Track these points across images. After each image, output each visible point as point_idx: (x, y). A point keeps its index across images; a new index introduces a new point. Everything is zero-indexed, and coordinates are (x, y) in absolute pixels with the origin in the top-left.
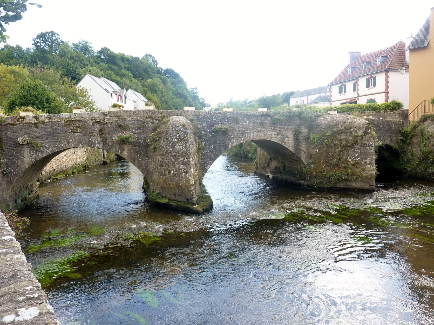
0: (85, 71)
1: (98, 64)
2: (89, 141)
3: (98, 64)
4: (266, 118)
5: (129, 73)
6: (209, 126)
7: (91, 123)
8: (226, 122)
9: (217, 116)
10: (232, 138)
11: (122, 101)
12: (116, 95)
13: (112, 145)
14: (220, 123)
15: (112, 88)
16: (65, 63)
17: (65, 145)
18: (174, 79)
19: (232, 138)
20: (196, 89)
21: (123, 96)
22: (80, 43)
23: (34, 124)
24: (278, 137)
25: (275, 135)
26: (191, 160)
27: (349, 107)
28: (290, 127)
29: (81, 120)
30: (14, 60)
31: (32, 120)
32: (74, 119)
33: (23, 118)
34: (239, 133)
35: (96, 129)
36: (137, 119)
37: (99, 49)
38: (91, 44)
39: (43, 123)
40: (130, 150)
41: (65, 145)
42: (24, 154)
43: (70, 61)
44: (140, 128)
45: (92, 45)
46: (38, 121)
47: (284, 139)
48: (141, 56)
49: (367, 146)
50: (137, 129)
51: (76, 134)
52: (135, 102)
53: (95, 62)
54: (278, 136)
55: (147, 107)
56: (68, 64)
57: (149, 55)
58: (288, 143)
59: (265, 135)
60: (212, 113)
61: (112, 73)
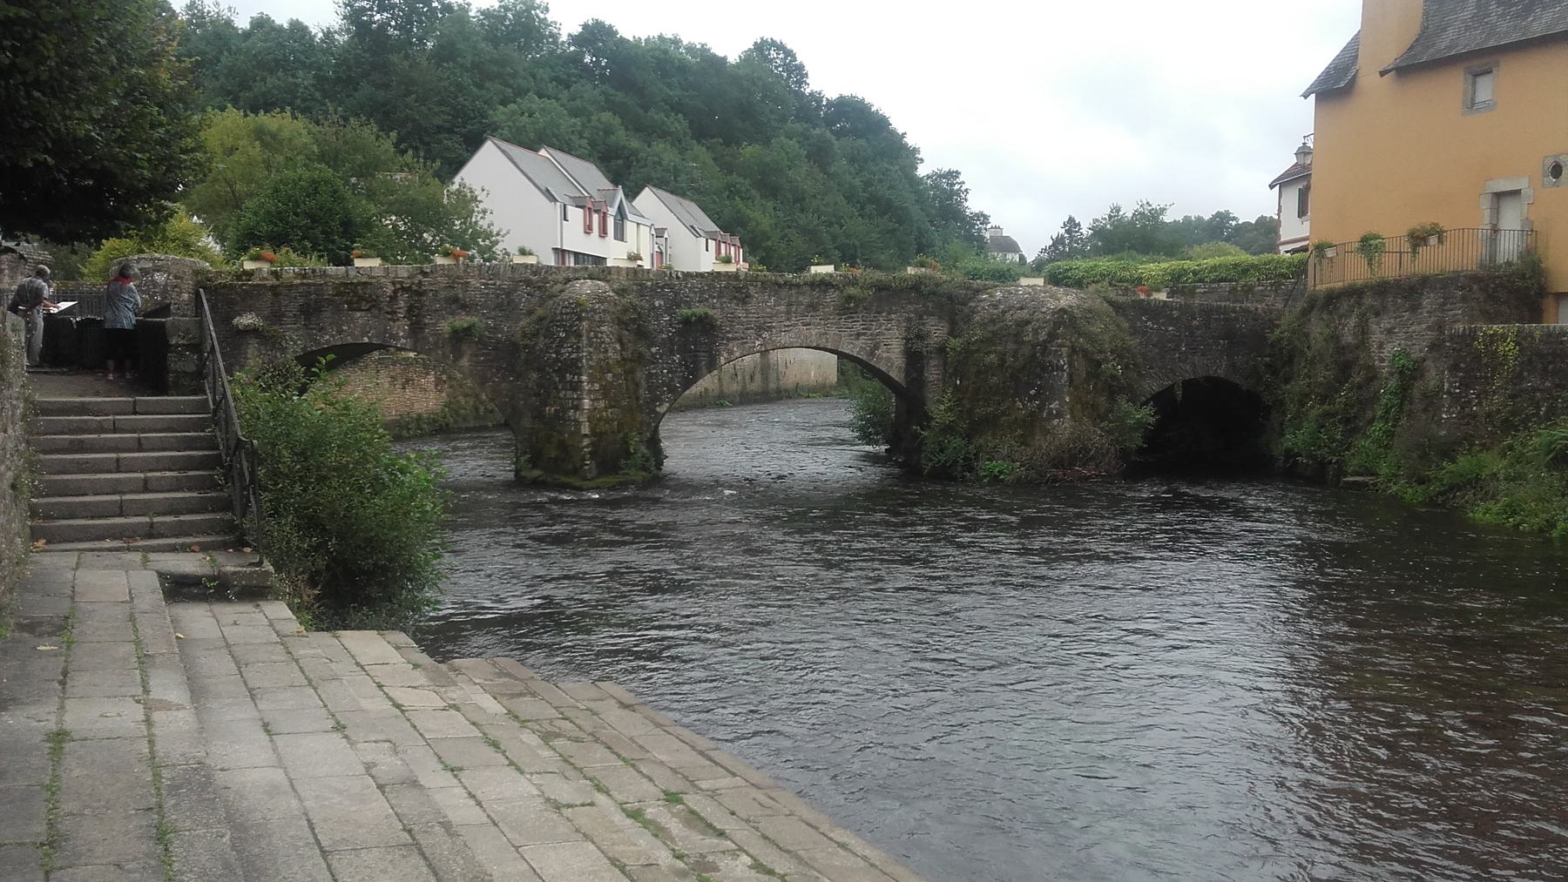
0: (513, 113)
1: (568, 87)
2: (386, 331)
3: (568, 87)
4: (825, 292)
5: (678, 124)
6: (671, 308)
7: (389, 290)
8: (714, 298)
9: (692, 284)
10: (729, 339)
11: (603, 233)
12: (581, 210)
13: (436, 343)
14: (699, 302)
15: (573, 181)
16: (446, 83)
17: (333, 336)
18: (861, 142)
19: (729, 339)
20: (952, 175)
21: (612, 211)
22: (507, 9)
23: (273, 288)
24: (860, 343)
25: (851, 335)
26: (584, 378)
27: (1236, 266)
28: (893, 316)
29: (371, 283)
30: (280, 74)
31: (266, 279)
32: (355, 281)
33: (250, 274)
34: (747, 329)
35: (402, 304)
36: (494, 284)
37: (576, 30)
38: (547, 10)
39: (290, 286)
40: (476, 356)
41: (333, 336)
42: (246, 353)
43: (467, 80)
44: (499, 307)
45: (550, 17)
46: (278, 283)
47: (876, 347)
48: (731, 47)
49: (1053, 370)
50: (494, 309)
51: (358, 314)
52: (659, 233)
53: (556, 79)
54: (858, 339)
55: (522, 257)
56: (460, 88)
57: (773, 43)
58: (889, 359)
59: (821, 334)
60: (680, 275)
61: (617, 121)
